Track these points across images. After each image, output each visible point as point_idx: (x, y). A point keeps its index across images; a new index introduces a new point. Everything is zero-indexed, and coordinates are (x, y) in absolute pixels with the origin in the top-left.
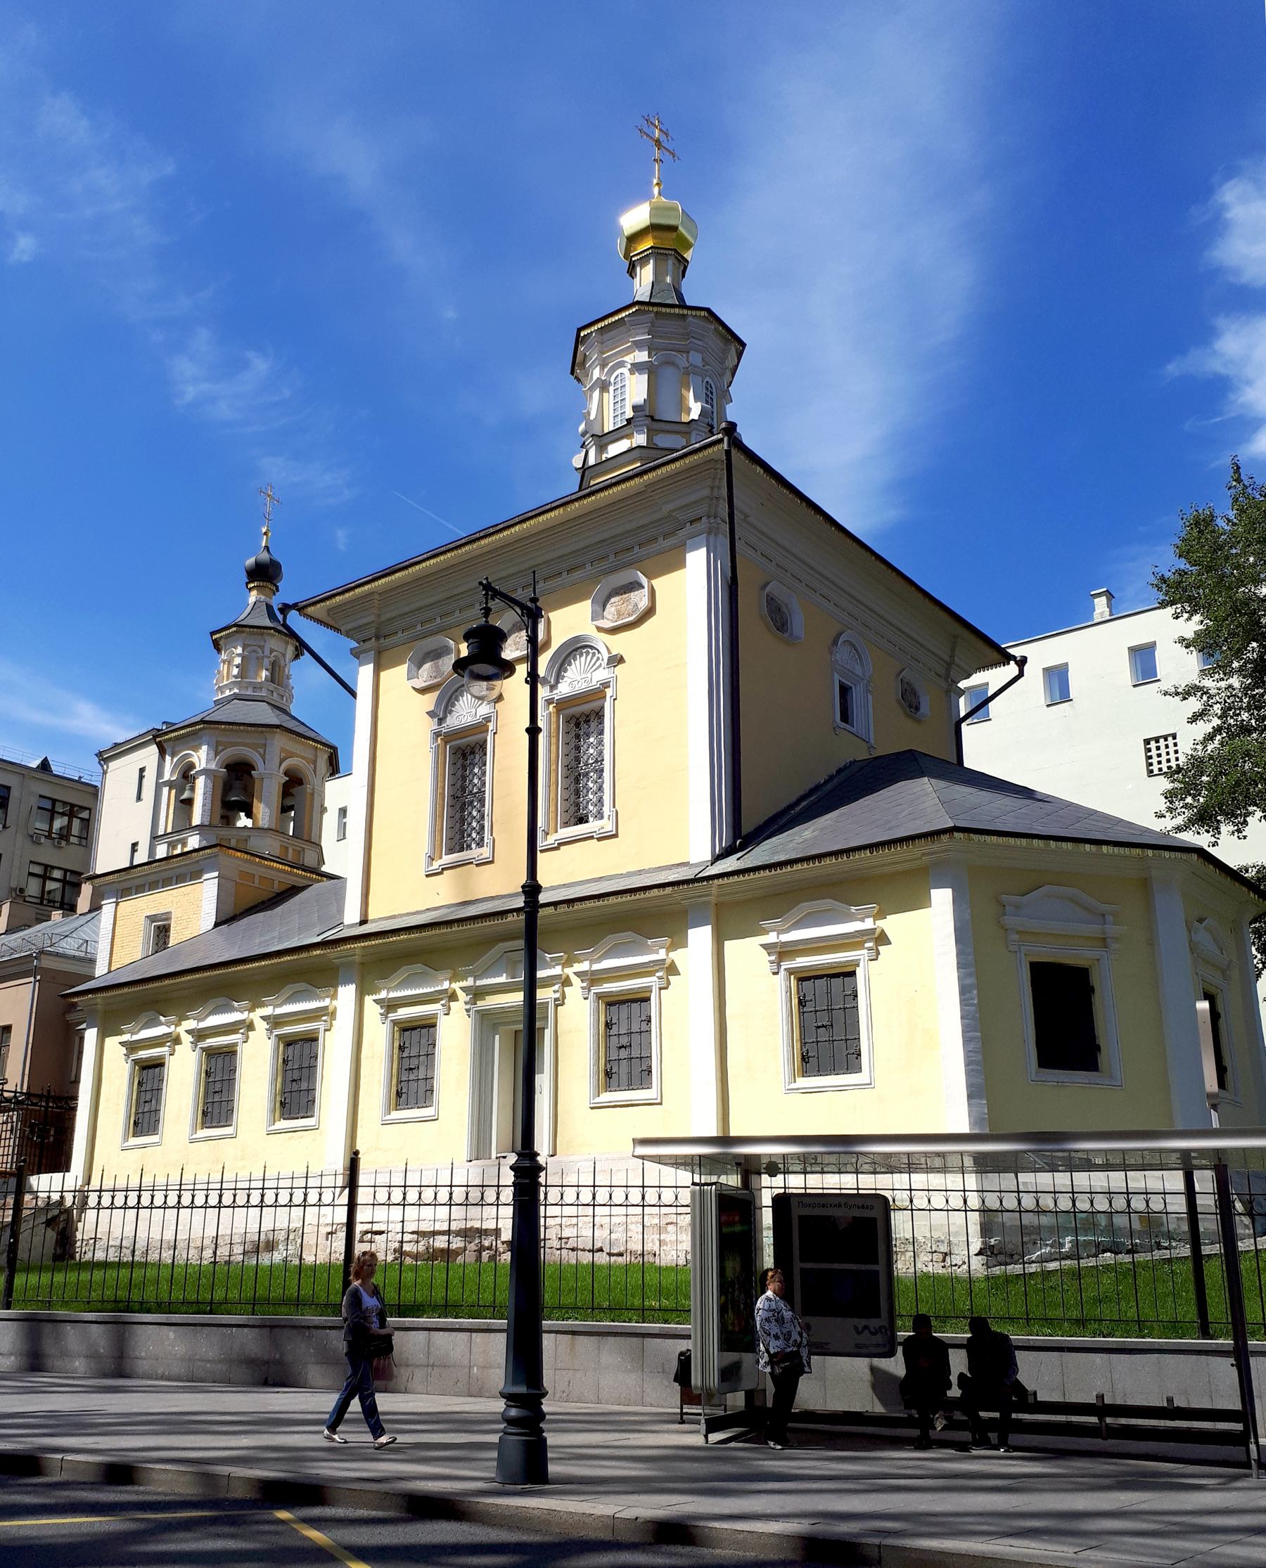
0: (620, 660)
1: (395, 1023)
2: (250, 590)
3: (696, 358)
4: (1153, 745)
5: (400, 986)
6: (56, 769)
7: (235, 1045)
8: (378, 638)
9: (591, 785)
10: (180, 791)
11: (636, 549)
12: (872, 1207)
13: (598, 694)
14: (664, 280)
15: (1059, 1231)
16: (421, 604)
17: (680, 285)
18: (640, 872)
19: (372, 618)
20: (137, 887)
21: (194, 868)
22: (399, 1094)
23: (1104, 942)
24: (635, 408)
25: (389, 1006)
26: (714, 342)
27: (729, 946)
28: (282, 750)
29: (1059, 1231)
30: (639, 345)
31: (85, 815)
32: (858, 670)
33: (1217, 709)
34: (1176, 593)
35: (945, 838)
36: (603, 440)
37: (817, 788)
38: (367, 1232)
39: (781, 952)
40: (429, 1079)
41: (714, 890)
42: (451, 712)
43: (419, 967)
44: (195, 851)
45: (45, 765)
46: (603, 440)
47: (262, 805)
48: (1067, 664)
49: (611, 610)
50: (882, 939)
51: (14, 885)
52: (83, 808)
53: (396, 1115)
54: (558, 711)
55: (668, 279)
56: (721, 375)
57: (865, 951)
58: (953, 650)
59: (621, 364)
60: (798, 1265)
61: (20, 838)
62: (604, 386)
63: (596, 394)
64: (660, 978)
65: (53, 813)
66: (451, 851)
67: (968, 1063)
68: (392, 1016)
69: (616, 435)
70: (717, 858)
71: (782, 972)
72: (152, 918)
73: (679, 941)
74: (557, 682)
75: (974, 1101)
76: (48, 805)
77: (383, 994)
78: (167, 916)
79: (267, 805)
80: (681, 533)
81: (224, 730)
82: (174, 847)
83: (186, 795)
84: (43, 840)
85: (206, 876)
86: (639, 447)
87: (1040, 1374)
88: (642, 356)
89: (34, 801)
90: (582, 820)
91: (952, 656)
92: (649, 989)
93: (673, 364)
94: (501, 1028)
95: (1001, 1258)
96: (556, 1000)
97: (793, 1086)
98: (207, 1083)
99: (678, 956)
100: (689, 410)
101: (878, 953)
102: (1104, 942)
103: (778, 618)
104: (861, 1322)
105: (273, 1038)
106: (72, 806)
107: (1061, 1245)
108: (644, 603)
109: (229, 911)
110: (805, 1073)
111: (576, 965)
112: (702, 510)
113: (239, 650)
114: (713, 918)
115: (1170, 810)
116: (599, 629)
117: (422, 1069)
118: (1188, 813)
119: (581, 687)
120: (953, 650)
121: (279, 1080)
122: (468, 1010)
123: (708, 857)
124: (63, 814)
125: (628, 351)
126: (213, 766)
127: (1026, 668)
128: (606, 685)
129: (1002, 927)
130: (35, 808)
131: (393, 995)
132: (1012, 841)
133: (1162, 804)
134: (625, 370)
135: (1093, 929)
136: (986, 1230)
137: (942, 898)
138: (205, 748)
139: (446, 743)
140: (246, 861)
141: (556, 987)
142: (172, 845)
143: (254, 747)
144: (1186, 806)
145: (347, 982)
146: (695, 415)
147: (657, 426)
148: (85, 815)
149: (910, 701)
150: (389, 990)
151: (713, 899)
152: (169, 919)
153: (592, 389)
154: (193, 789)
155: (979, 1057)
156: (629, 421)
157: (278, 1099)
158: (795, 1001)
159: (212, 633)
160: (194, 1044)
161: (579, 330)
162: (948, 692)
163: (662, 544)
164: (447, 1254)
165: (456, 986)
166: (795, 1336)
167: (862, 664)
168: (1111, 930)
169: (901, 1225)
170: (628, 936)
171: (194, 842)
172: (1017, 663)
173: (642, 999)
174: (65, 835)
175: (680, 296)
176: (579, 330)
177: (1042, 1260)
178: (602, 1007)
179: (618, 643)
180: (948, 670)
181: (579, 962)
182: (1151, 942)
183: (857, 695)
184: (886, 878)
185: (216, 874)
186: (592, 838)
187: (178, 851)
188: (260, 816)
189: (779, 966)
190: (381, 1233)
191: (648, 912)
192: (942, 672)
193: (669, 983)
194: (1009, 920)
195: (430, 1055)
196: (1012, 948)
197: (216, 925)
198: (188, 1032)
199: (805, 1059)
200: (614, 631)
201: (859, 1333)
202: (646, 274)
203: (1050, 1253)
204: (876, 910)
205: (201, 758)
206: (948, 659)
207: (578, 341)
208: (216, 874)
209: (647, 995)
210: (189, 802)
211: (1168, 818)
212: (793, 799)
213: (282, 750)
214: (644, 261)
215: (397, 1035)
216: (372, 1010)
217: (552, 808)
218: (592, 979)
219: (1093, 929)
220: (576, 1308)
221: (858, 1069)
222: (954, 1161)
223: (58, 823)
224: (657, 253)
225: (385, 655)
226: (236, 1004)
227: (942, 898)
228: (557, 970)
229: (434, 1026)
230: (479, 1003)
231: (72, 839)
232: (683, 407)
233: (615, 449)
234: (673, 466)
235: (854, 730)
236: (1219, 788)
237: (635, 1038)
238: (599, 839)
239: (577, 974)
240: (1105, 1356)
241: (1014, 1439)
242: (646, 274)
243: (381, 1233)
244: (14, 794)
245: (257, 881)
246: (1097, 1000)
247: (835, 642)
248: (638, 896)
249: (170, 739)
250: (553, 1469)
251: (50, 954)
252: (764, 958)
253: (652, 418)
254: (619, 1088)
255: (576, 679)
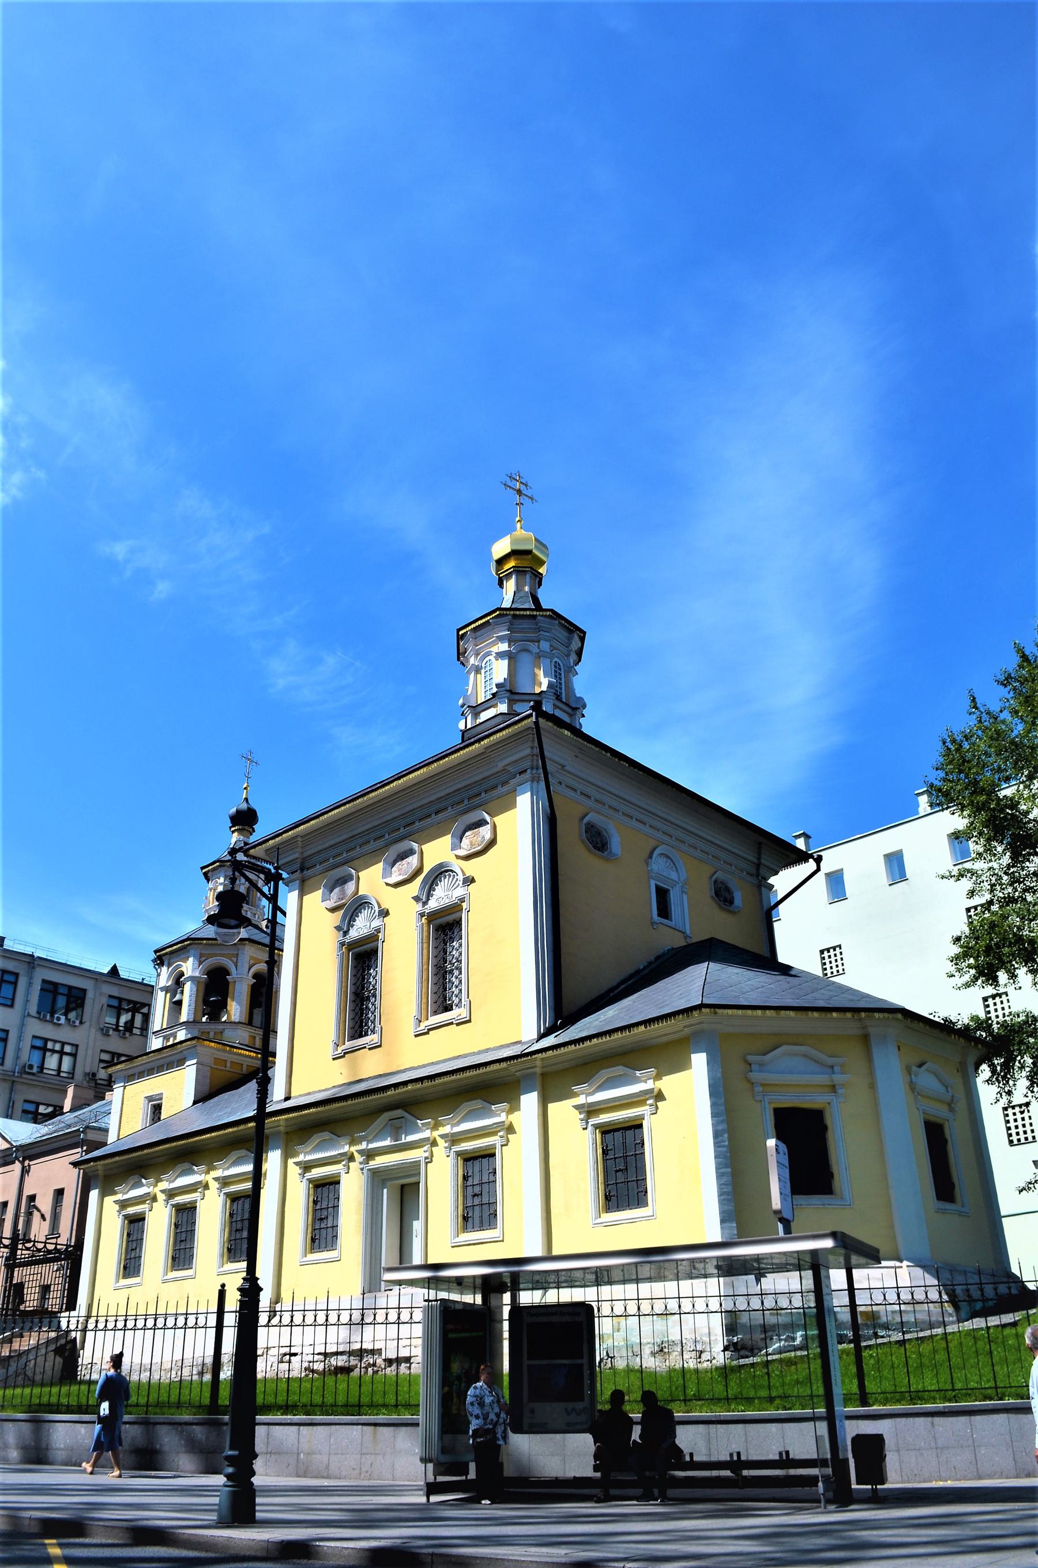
0: (473, 880)
1: (310, 1181)
2: (233, 832)
3: (545, 646)
4: (826, 954)
5: (315, 1149)
6: (123, 974)
7: (195, 1201)
8: (302, 870)
9: (454, 979)
10: (174, 995)
11: (483, 795)
12: (579, 1314)
13: (456, 908)
14: (523, 590)
15: (792, 1327)
16: (320, 848)
17: (536, 592)
18: (487, 1050)
19: (297, 855)
20: (139, 1073)
21: (178, 1057)
22: (313, 1240)
23: (833, 1088)
24: (498, 686)
25: (306, 1167)
26: (562, 634)
27: (552, 1107)
28: (252, 958)
29: (792, 1327)
30: (501, 639)
31: (145, 1010)
32: (674, 876)
33: (986, 886)
34: (943, 798)
35: (696, 1013)
36: (477, 710)
37: (638, 972)
38: (285, 1355)
39: (589, 1111)
40: (335, 1227)
41: (538, 1063)
42: (353, 926)
43: (326, 1135)
44: (181, 1042)
45: (114, 971)
46: (477, 710)
47: (234, 1003)
48: (901, 851)
49: (465, 842)
50: (660, 1096)
51: (87, 1071)
52: (144, 1005)
53: (311, 1257)
54: (429, 922)
55: (527, 589)
56: (568, 656)
57: (648, 1107)
58: (759, 853)
59: (489, 654)
60: (526, 1362)
61: (93, 1030)
62: (478, 670)
63: (472, 675)
64: (501, 1137)
65: (119, 1011)
66: (352, 1038)
67: (721, 1194)
68: (308, 1175)
69: (486, 705)
70: (541, 1037)
71: (590, 1128)
72: (150, 1099)
73: (515, 1107)
74: (428, 899)
75: (725, 1225)
76: (115, 1003)
77: (301, 1158)
78: (160, 1097)
79: (239, 1003)
80: (513, 782)
81: (206, 944)
82: (168, 1040)
83: (177, 998)
84: (111, 1032)
85: (188, 1063)
86: (501, 714)
87: (689, 1439)
88: (504, 647)
89: (104, 1000)
90: (448, 1008)
91: (759, 859)
92: (494, 1147)
93: (528, 651)
94: (389, 1183)
95: (743, 1353)
96: (426, 1158)
97: (599, 1221)
98: (176, 1234)
99: (515, 1118)
100: (540, 684)
101: (657, 1108)
102: (833, 1088)
103: (597, 840)
104: (570, 1406)
105: (222, 1195)
106: (135, 1003)
107: (794, 1339)
108: (488, 836)
109: (206, 1089)
110: (608, 1209)
111: (440, 1128)
112: (527, 764)
113: (222, 880)
114: (538, 1086)
115: (959, 970)
116: (458, 857)
117: (330, 1219)
118: (973, 971)
119: (445, 902)
120: (759, 853)
121: (227, 1230)
122: (362, 1169)
123: (534, 1035)
124: (127, 1011)
125: (494, 644)
126: (197, 974)
127: (822, 864)
128: (462, 900)
129: (749, 1081)
130: (105, 1007)
131: (309, 1157)
132: (749, 1012)
133: (951, 968)
134: (491, 657)
135: (823, 1079)
136: (731, 1329)
137: (699, 1060)
138: (191, 959)
139: (349, 951)
140: (218, 1050)
141: (425, 1148)
142: (166, 1038)
143: (229, 957)
144: (970, 966)
145: (274, 1148)
146: (544, 688)
147: (516, 697)
148: (145, 1010)
149: (723, 895)
150: (306, 1153)
151: (538, 1070)
152: (161, 1099)
153: (469, 673)
154: (182, 992)
155: (729, 1189)
156: (494, 695)
157: (226, 1245)
158: (600, 1151)
159: (202, 868)
160: (167, 1201)
161: (459, 630)
162: (759, 886)
163: (501, 790)
164: (347, 1370)
165: (353, 1149)
166: (492, 1416)
167: (677, 871)
168: (838, 1078)
169: (604, 1326)
170: (477, 1104)
171: (182, 1035)
172: (815, 860)
173: (489, 1155)
174: (129, 1026)
175: (536, 600)
176: (459, 630)
177: (780, 1351)
178: (460, 1162)
179: (471, 868)
180: (758, 869)
181: (443, 1126)
182: (873, 1086)
183: (674, 897)
184: (655, 1050)
185: (195, 1061)
186: (452, 1023)
187: (171, 1042)
188: (232, 1013)
189: (587, 1123)
190: (295, 1355)
191: (485, 1084)
192: (753, 871)
193: (508, 1141)
194: (755, 1076)
195: (336, 1207)
196: (759, 1098)
197: (195, 1103)
198: (162, 1191)
199: (608, 1198)
200: (468, 858)
201: (568, 1414)
202: (511, 585)
203: (784, 1346)
204: (654, 1073)
205: (189, 967)
206: (755, 861)
207: (460, 638)
208: (195, 1061)
209: (492, 1151)
210: (179, 1003)
211: (957, 977)
212: (615, 984)
213: (252, 958)
214: (508, 576)
215: (312, 1192)
216: (294, 1171)
217: (424, 1000)
218: (453, 1139)
219: (823, 1079)
220: (385, 1406)
221: (646, 1205)
222: (616, 1275)
223: (124, 1018)
224: (518, 571)
225: (308, 883)
226: (195, 1168)
227: (699, 1060)
228: (427, 1134)
229: (338, 1183)
230: (371, 1163)
231: (135, 1031)
232: (534, 680)
233: (485, 716)
234: (501, 734)
235: (672, 924)
236: (989, 951)
237: (485, 1187)
238: (458, 1024)
239: (442, 1136)
240: (779, 1425)
241: (671, 1492)
242: (511, 585)
243: (295, 1355)
244: (90, 995)
245: (228, 1065)
246: (830, 1134)
247: (650, 856)
248: (482, 1070)
249: (166, 954)
250: (259, 1515)
251: (94, 1128)
252: (577, 1116)
253: (511, 692)
254: (474, 1229)
255: (442, 896)
